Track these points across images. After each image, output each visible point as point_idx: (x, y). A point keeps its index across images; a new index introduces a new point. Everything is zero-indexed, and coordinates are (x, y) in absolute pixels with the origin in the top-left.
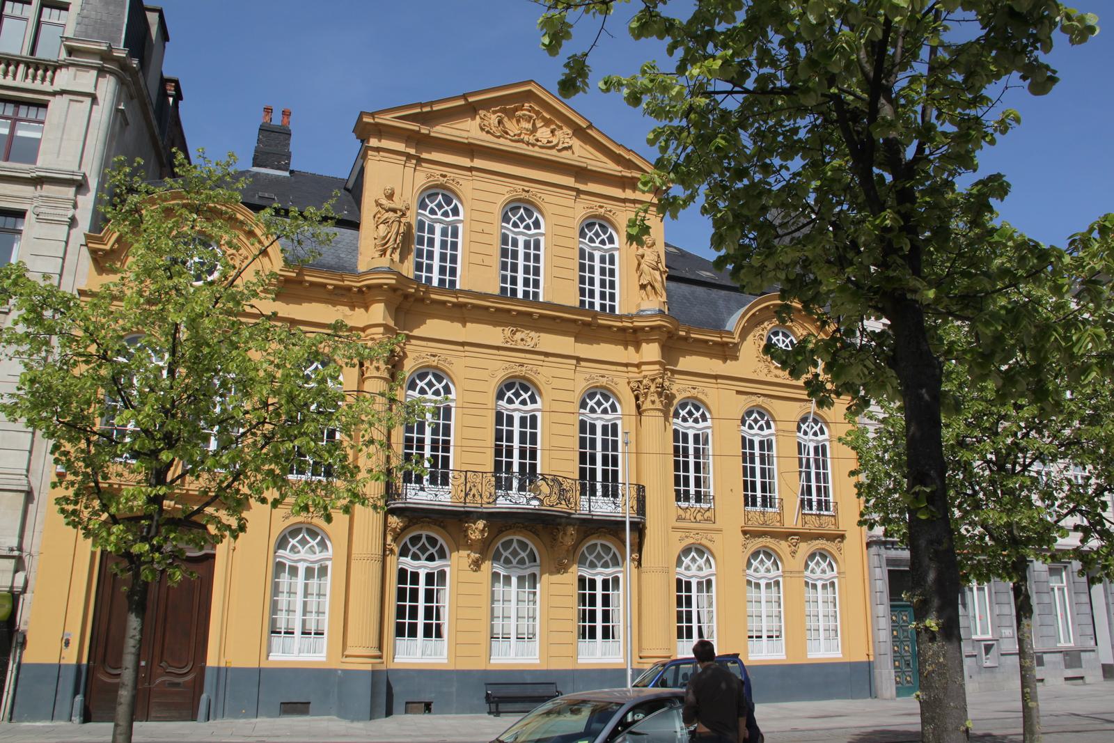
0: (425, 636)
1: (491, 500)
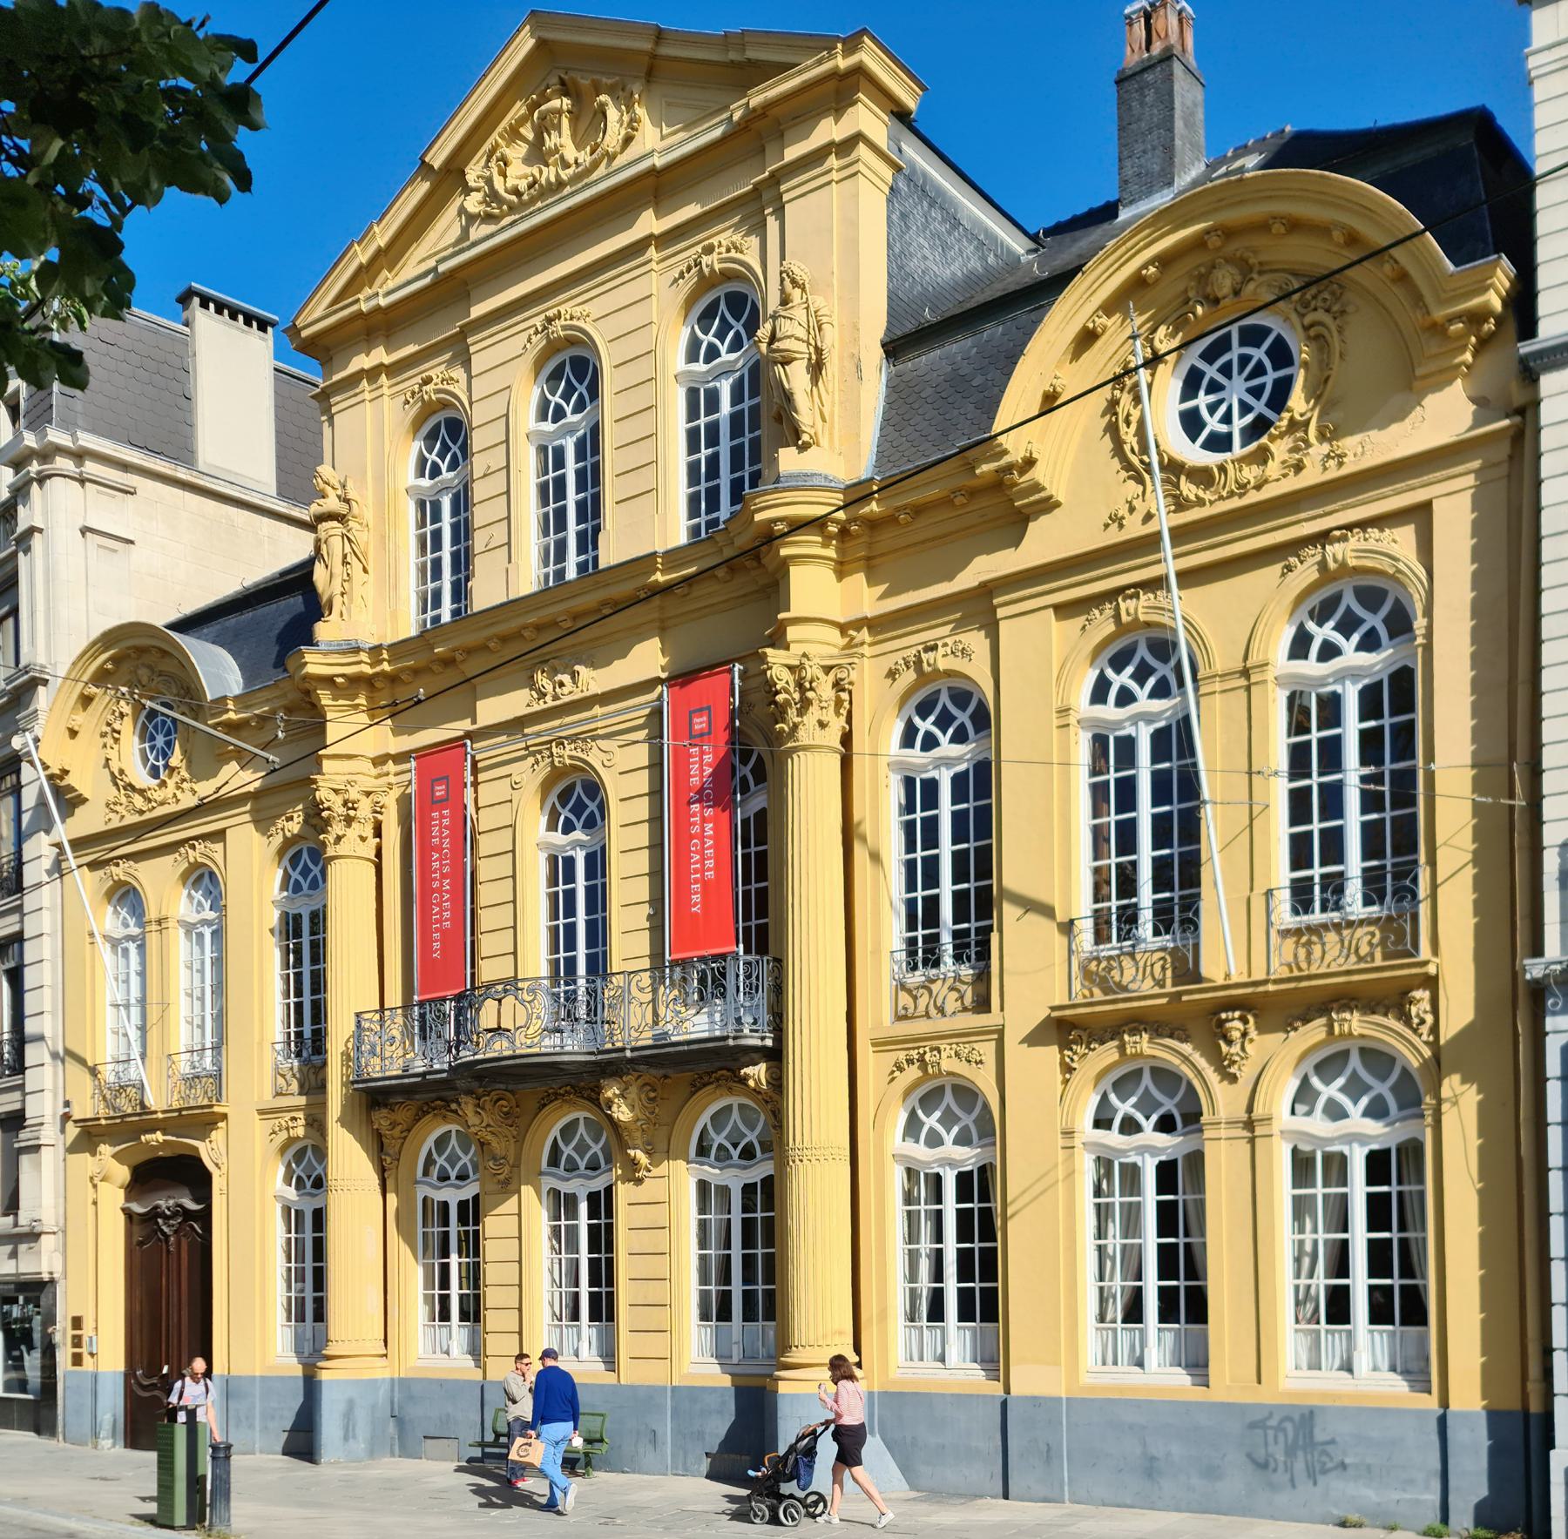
0: (1162, 1319)
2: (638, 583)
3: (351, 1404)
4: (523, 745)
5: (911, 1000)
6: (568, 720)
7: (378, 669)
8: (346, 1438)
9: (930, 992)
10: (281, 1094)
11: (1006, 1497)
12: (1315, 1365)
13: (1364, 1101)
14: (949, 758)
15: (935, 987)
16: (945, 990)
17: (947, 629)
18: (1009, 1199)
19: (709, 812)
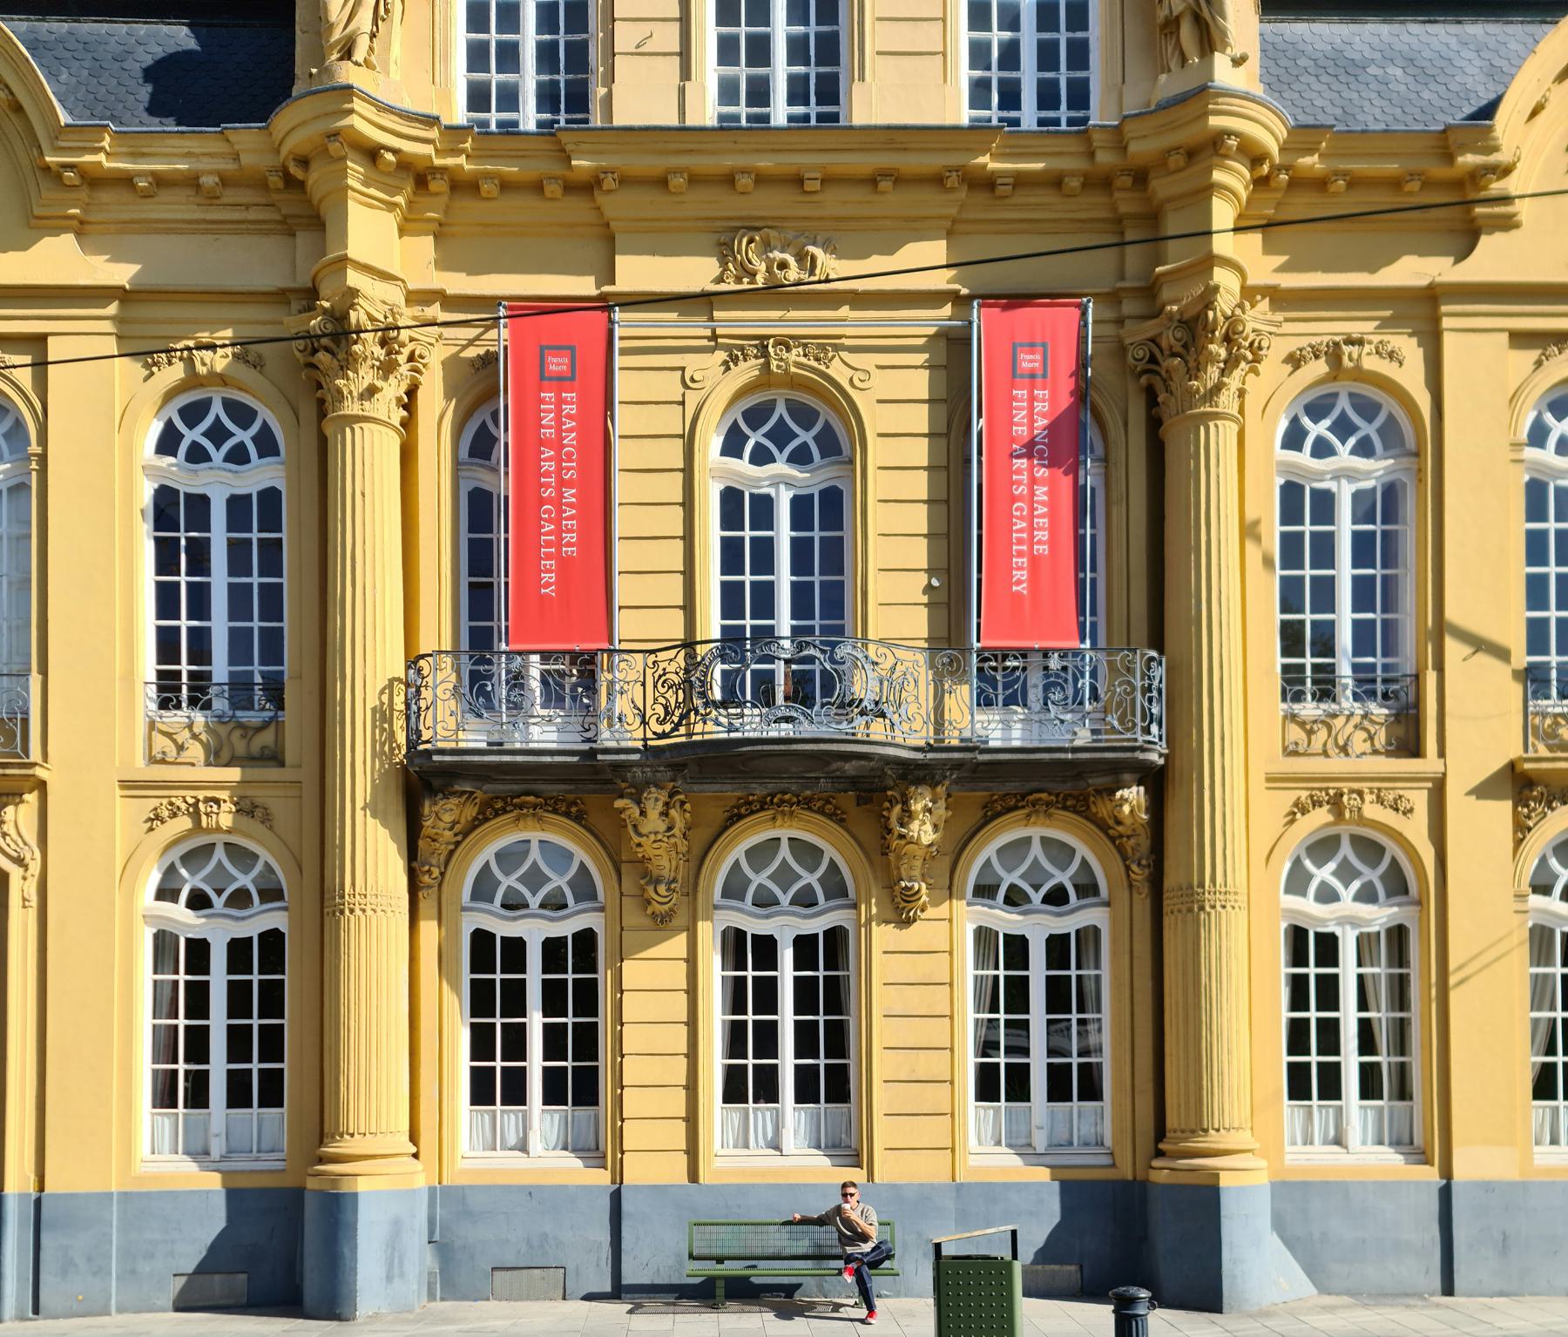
0: (1052, 1097)
1: (668, 727)
2: (953, 160)
3: (397, 1226)
4: (708, 333)
5: (1303, 735)
6: (793, 314)
7: (450, 161)
8: (389, 1278)
9: (1329, 728)
10: (1295, 753)
11: (564, 1298)
12: (1308, 1141)
13: (1356, 885)
14: (1349, 474)
15: (1338, 722)
16: (1349, 728)
17: (1370, 326)
18: (1452, 966)
19: (1042, 473)
